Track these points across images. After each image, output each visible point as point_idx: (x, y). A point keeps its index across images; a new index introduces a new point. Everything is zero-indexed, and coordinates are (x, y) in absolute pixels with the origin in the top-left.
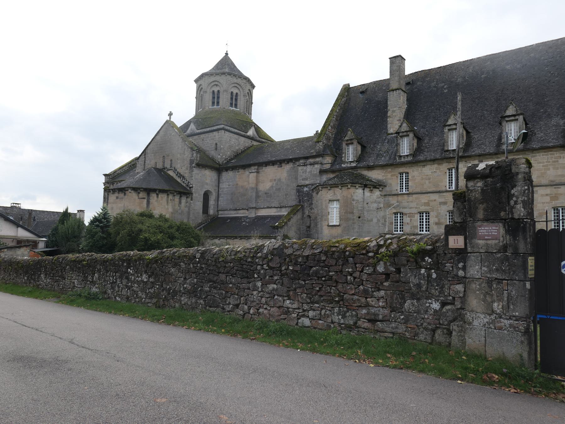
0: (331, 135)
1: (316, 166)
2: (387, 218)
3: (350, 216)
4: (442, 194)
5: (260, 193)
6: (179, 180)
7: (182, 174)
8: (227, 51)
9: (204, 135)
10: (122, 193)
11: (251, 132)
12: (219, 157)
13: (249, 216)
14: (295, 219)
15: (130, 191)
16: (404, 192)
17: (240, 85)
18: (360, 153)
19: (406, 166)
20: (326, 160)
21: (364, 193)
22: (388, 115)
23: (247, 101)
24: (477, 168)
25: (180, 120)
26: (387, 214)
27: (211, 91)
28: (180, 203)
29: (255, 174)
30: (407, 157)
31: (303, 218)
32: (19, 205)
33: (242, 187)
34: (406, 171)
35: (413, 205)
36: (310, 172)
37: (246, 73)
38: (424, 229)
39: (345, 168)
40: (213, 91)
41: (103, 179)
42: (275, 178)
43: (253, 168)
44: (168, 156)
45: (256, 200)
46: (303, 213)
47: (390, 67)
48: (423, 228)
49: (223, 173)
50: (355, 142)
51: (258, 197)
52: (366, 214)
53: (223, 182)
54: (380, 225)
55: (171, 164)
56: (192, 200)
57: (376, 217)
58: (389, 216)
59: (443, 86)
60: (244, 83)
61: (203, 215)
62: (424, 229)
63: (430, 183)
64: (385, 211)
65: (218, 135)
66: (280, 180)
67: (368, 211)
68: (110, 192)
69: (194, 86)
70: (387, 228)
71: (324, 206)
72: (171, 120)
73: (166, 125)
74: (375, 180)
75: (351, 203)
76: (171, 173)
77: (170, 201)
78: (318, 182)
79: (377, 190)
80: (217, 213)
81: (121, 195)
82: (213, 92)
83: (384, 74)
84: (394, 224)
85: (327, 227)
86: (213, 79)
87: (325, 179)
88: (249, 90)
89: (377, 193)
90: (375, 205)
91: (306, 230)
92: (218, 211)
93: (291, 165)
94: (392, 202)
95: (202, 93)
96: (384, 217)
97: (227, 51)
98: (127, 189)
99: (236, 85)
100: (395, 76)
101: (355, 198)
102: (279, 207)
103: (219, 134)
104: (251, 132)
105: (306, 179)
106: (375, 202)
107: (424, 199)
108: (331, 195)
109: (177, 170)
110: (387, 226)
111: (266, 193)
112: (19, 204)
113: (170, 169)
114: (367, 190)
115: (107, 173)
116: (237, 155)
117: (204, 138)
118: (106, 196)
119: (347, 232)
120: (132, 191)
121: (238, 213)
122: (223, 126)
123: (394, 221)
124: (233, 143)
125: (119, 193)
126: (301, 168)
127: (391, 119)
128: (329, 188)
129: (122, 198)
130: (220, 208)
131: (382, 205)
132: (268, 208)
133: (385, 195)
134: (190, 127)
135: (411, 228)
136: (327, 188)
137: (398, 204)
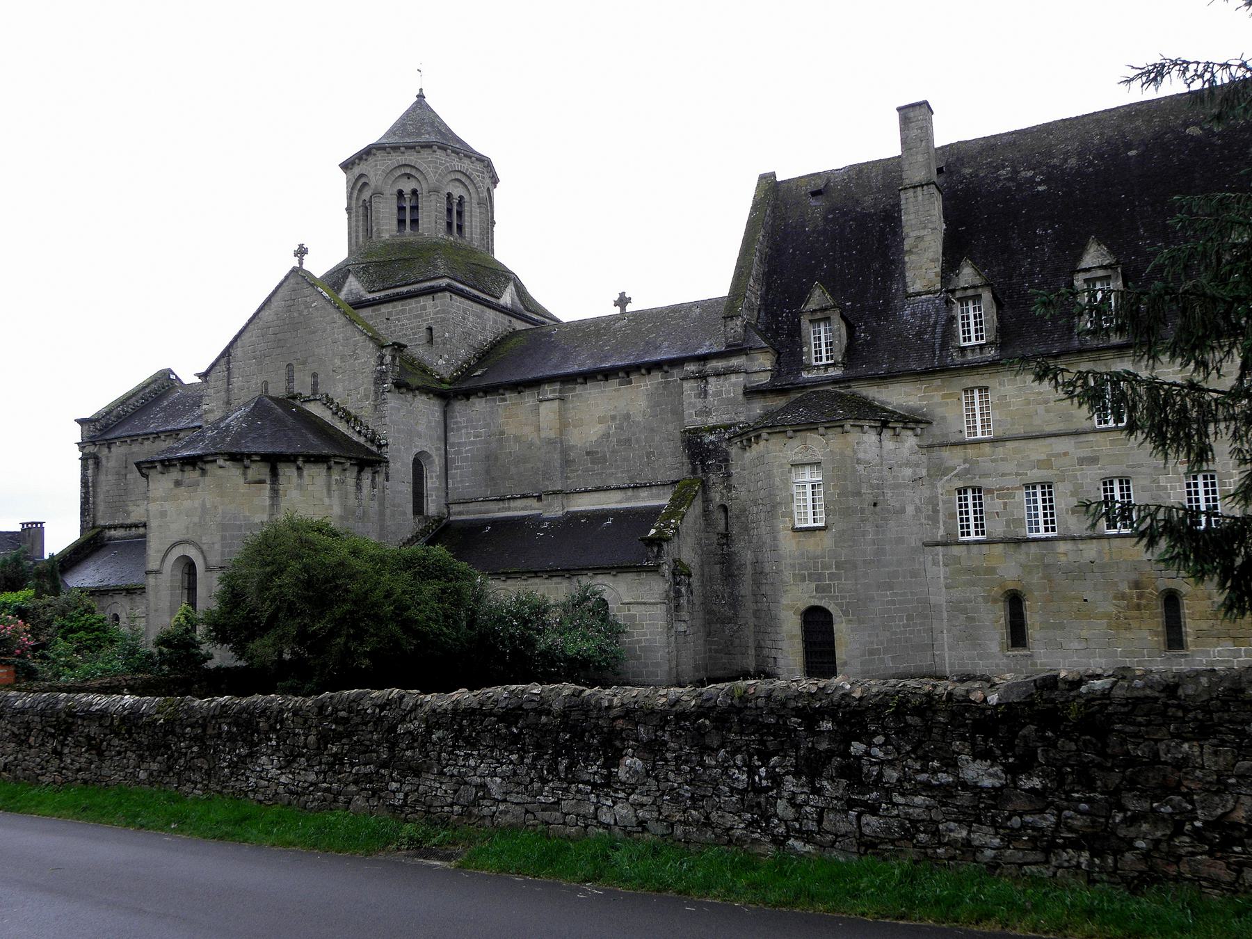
1: (733, 378)
2: (940, 504)
3: (854, 502)
4: (1083, 438)
6: (341, 427)
7: (353, 411)
8: (421, 90)
9: (390, 305)
10: (194, 469)
11: (507, 298)
12: (440, 362)
13: (546, 515)
14: (694, 512)
15: (221, 462)
16: (979, 436)
18: (845, 342)
19: (981, 371)
20: (756, 363)
21: (880, 441)
22: (906, 248)
25: (320, 265)
26: (940, 491)
28: (358, 486)
29: (556, 403)
30: (826, 370)
31: (706, 513)
33: (517, 439)
34: (982, 383)
35: (1010, 467)
36: (718, 393)
37: (479, 145)
38: (972, 529)
39: (808, 380)
41: (76, 433)
43: (547, 388)
45: (562, 473)
46: (707, 501)
47: (902, 130)
48: (968, 527)
49: (458, 403)
50: (836, 317)
51: (567, 462)
52: (890, 494)
53: (459, 429)
54: (923, 520)
55: (315, 384)
56: (387, 480)
57: (913, 501)
58: (944, 497)
59: (1034, 177)
60: (477, 171)
62: (972, 529)
63: (1047, 411)
64: (933, 486)
65: (435, 306)
66: (627, 417)
67: (895, 487)
68: (156, 467)
69: (340, 181)
70: (942, 526)
71: (777, 479)
72: (304, 267)
73: (292, 281)
74: (900, 410)
75: (855, 471)
76: (316, 409)
77: (334, 487)
78: (742, 419)
79: (910, 433)
80: (445, 511)
81: (192, 475)
82: (400, 194)
83: (889, 146)
84: (958, 517)
85: (790, 532)
86: (397, 158)
88: (488, 189)
89: (910, 440)
90: (908, 472)
92: (447, 505)
93: (657, 377)
94: (950, 463)
95: (366, 195)
96: (933, 502)
97: (421, 90)
98: (210, 458)
99: (459, 176)
100: (917, 153)
101: (861, 455)
102: (630, 487)
103: (437, 301)
104: (507, 298)
106: (907, 464)
107: (1037, 450)
109: (335, 401)
110: (941, 523)
111: (588, 453)
113: (312, 398)
114: (887, 433)
115: (88, 416)
116: (488, 355)
117: (390, 313)
118: (90, 479)
119: (851, 543)
120: (228, 463)
121: (509, 509)
122: (446, 281)
123: (958, 510)
125: (182, 471)
126: (690, 385)
127: (913, 257)
128: (790, 433)
130: (450, 500)
131: (924, 472)
132: (598, 490)
134: (347, 284)
135: (1008, 525)
136: (783, 435)
137: (967, 466)
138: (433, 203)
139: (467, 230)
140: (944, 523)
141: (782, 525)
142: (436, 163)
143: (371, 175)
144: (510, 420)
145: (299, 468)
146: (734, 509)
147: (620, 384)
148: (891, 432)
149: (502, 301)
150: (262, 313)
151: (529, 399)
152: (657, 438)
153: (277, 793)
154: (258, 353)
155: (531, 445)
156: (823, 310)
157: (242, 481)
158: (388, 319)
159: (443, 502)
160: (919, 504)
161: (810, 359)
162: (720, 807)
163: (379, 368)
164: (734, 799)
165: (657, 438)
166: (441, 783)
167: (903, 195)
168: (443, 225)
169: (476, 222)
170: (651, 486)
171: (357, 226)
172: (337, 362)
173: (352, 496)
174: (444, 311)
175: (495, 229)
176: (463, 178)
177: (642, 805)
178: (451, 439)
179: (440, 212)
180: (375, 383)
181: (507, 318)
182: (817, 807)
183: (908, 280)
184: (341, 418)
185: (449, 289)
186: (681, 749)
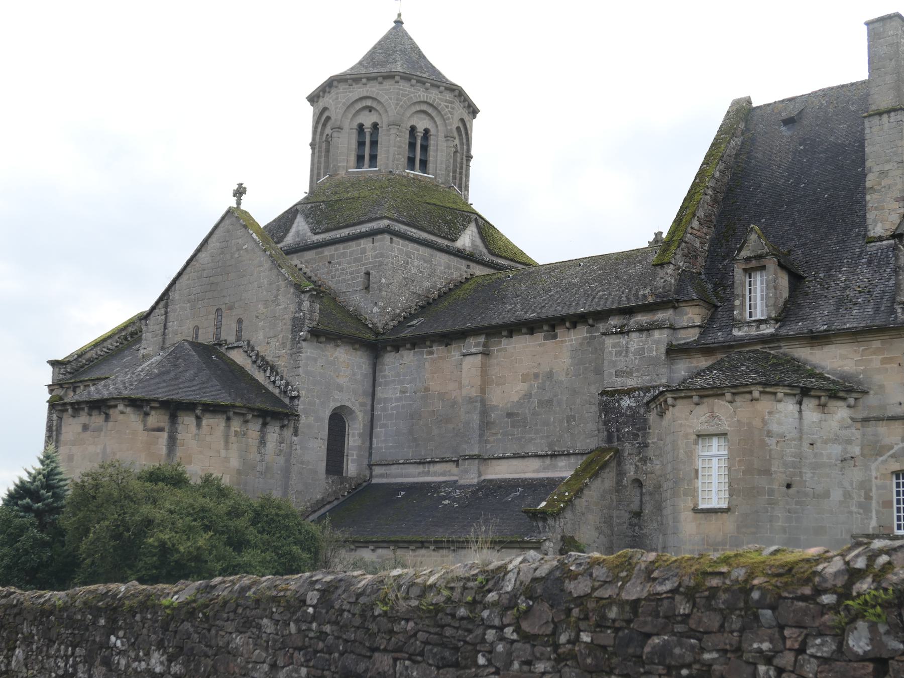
0: (698, 245)
1: (657, 334)
3: (762, 482)
6: (260, 377)
7: (268, 358)
8: (399, 15)
11: (467, 239)
12: (375, 309)
15: (121, 407)
18: (786, 294)
20: (685, 318)
21: (800, 412)
22: (868, 184)
23: (456, 152)
26: (874, 474)
27: (355, 125)
28: (263, 442)
31: (619, 488)
33: (441, 396)
36: (640, 352)
39: (741, 339)
40: (361, 127)
41: (47, 375)
42: (536, 371)
43: (472, 340)
44: (231, 308)
45: (481, 436)
46: (621, 474)
49: (388, 355)
50: (771, 264)
51: (486, 424)
55: (239, 331)
56: (296, 435)
60: (446, 101)
61: (327, 478)
65: (374, 249)
66: (550, 375)
68: (67, 410)
69: (308, 113)
71: (681, 451)
73: (227, 222)
76: (238, 357)
77: (233, 439)
78: (664, 381)
79: (840, 403)
80: (367, 473)
81: (97, 420)
84: (895, 506)
86: (359, 91)
87: (683, 373)
88: (462, 120)
89: (840, 412)
90: (836, 450)
92: (370, 466)
93: (581, 333)
95: (328, 131)
96: (865, 486)
97: (399, 15)
98: (112, 403)
99: (424, 107)
103: (377, 244)
104: (467, 239)
105: (629, 373)
106: (836, 440)
108: (703, 419)
111: (510, 415)
113: (236, 345)
117: (332, 256)
121: (428, 473)
122: (386, 222)
124: (414, 270)
125: (90, 415)
127: (876, 196)
128: (696, 399)
129: (99, 430)
130: (375, 458)
131: (856, 450)
132: (516, 456)
133: (866, 420)
134: (295, 225)
138: (392, 137)
140: (877, 512)
141: (685, 504)
143: (332, 108)
144: (436, 375)
145: (198, 418)
146: (649, 486)
147: (546, 338)
148: (815, 402)
149: (459, 244)
150: (199, 255)
151: (455, 353)
152: (578, 401)
154: (192, 297)
155: (454, 404)
156: (759, 257)
157: (141, 427)
158: (330, 263)
159: (366, 462)
160: (849, 488)
161: (741, 314)
165: (578, 401)
167: (867, 123)
168: (404, 160)
170: (569, 455)
171: (319, 162)
172: (261, 306)
173: (254, 449)
174: (382, 255)
175: (471, 164)
176: (427, 109)
178: (379, 394)
180: (293, 331)
181: (464, 262)
183: (869, 221)
184: (260, 367)
185: (387, 231)
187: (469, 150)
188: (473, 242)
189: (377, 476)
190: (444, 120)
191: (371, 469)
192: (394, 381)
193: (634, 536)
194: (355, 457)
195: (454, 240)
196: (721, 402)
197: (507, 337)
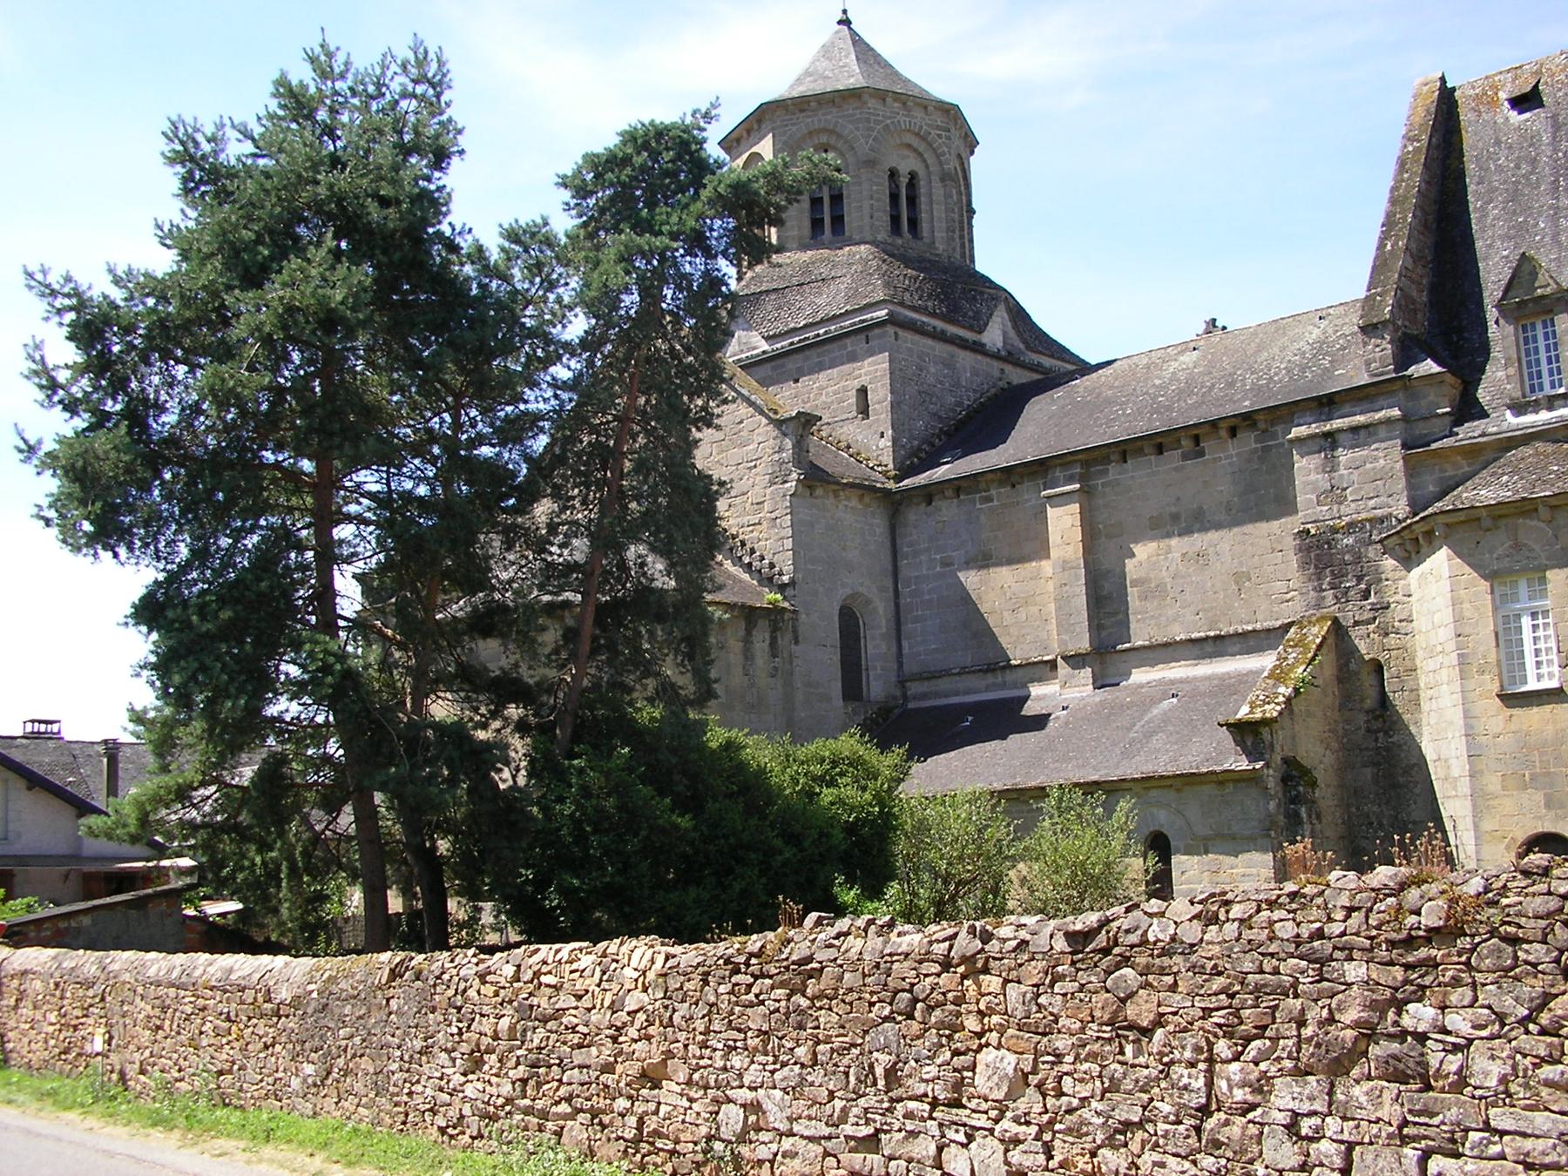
0: (1414, 294)
5: (1107, 586)
8: (845, 12)
11: (995, 334)
17: (924, 139)
24: (970, 579)
32: (55, 728)
42: (1174, 509)
60: (938, 128)
61: (846, 707)
87: (1431, 488)
88: (959, 156)
91: (1368, 730)
92: (902, 683)
97: (845, 12)
99: (915, 142)
108: (1500, 551)
112: (51, 722)
121: (1004, 686)
124: (931, 380)
130: (910, 667)
139: (925, 227)
142: (868, 120)
144: (1000, 534)
153: (462, 1117)
162: (1157, 1145)
163: (776, 457)
164: (1181, 1128)
166: (691, 1100)
169: (939, 211)
175: (974, 222)
177: (1017, 1141)
178: (906, 571)
179: (878, 200)
182: (1342, 1142)
186: (1083, 1030)
187: (969, 202)
188: (1005, 334)
189: (915, 698)
190: (938, 157)
191: (904, 687)
192: (928, 550)
193: (1378, 748)
194: (879, 671)
195: (980, 332)
196: (1534, 523)
197: (1117, 462)
